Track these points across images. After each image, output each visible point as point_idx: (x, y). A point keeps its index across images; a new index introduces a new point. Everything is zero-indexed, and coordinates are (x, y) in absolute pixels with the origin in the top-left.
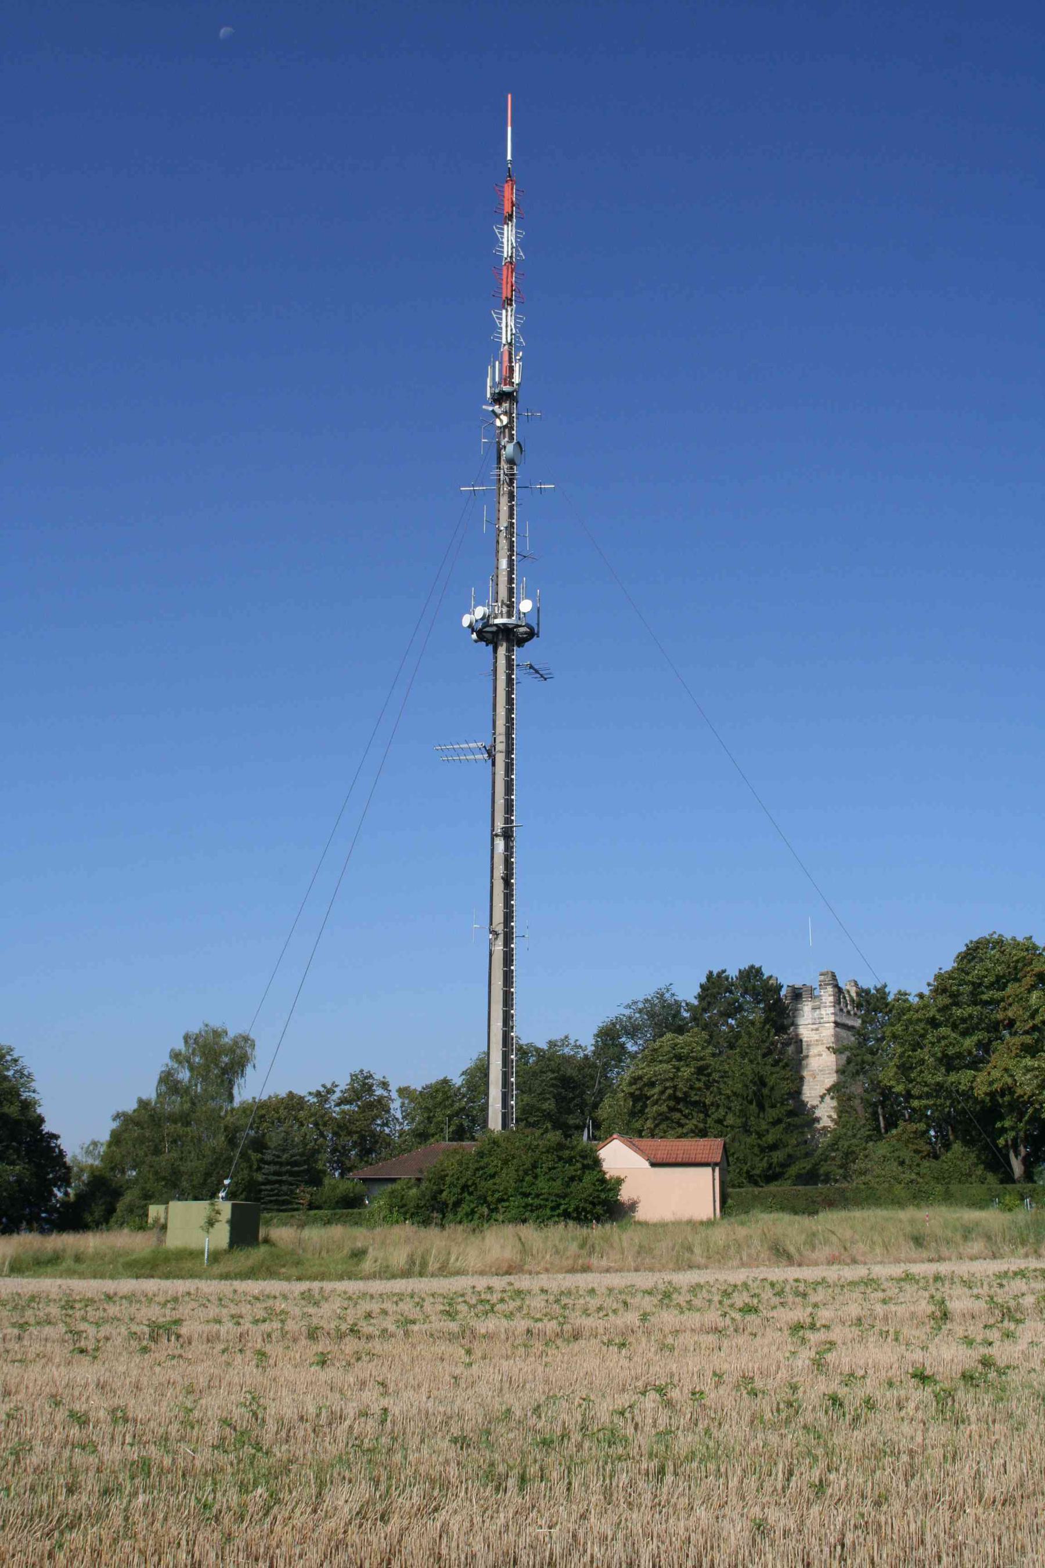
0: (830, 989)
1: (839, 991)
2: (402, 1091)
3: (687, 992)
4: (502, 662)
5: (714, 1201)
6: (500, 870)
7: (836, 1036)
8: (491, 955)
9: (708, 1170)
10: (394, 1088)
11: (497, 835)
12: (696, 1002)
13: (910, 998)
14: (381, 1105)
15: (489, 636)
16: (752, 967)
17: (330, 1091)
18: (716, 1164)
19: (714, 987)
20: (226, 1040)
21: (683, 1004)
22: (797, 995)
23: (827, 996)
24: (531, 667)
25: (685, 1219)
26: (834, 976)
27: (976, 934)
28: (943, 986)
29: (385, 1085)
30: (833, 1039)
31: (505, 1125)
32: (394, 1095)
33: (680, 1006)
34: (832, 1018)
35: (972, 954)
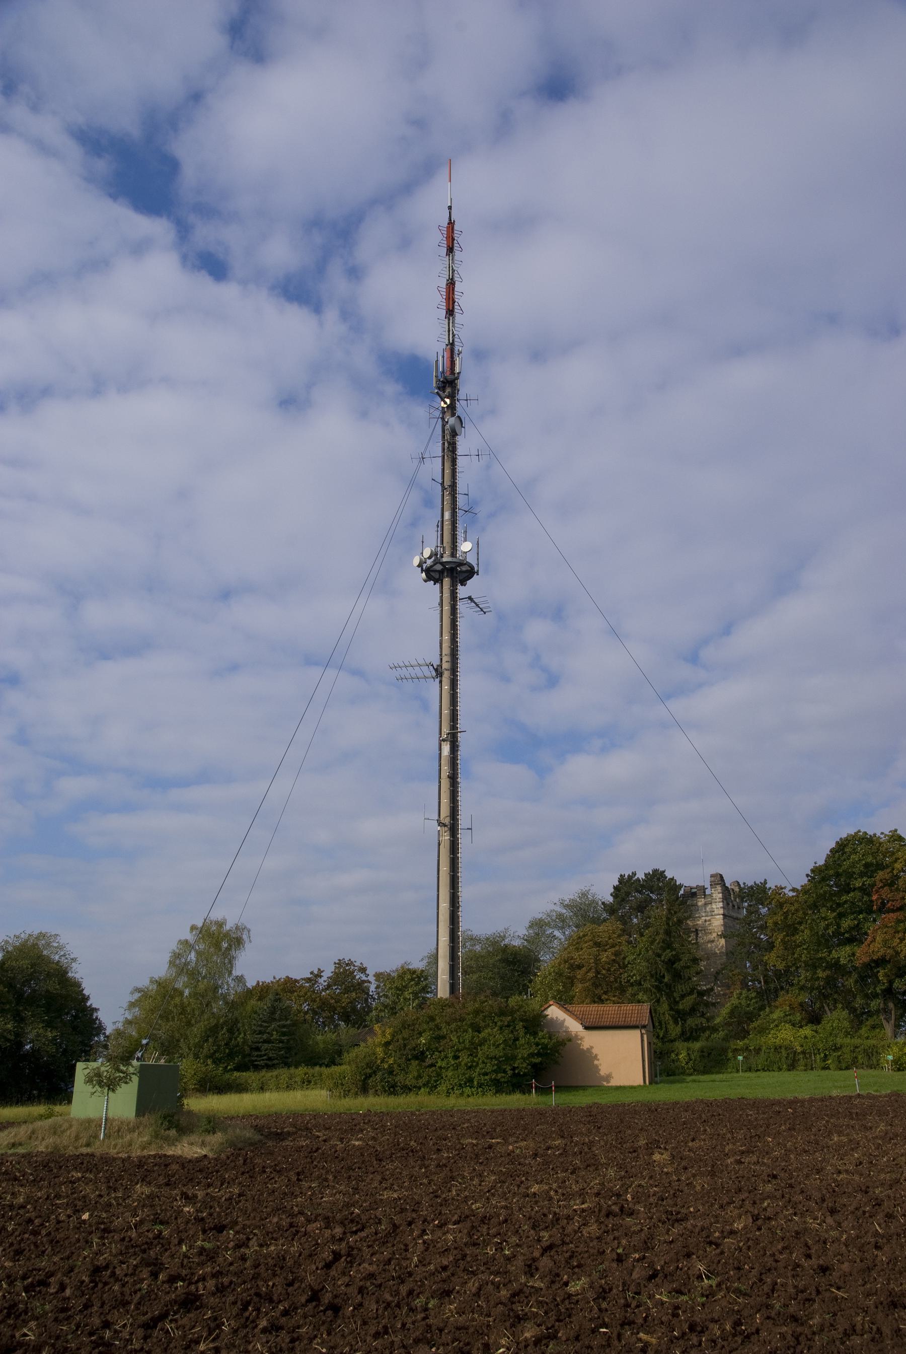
0: (719, 888)
1: (726, 891)
2: (378, 976)
3: (604, 892)
4: (447, 594)
5: (643, 1061)
6: (446, 769)
7: (725, 925)
8: (439, 845)
9: (636, 1034)
10: (371, 972)
11: (444, 740)
12: (611, 899)
13: (786, 891)
14: (361, 987)
15: (437, 576)
16: (655, 871)
17: (319, 975)
18: (644, 1027)
19: (626, 887)
20: (227, 927)
21: (600, 903)
22: (692, 894)
23: (718, 895)
24: (470, 598)
25: (242, 1112)
26: (721, 876)
27: (846, 831)
28: (819, 875)
29: (363, 970)
30: (722, 928)
31: (453, 988)
32: (371, 978)
33: (597, 904)
34: (721, 911)
35: (842, 848)
